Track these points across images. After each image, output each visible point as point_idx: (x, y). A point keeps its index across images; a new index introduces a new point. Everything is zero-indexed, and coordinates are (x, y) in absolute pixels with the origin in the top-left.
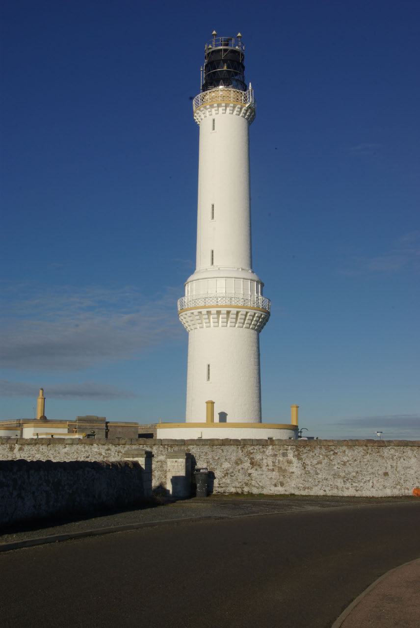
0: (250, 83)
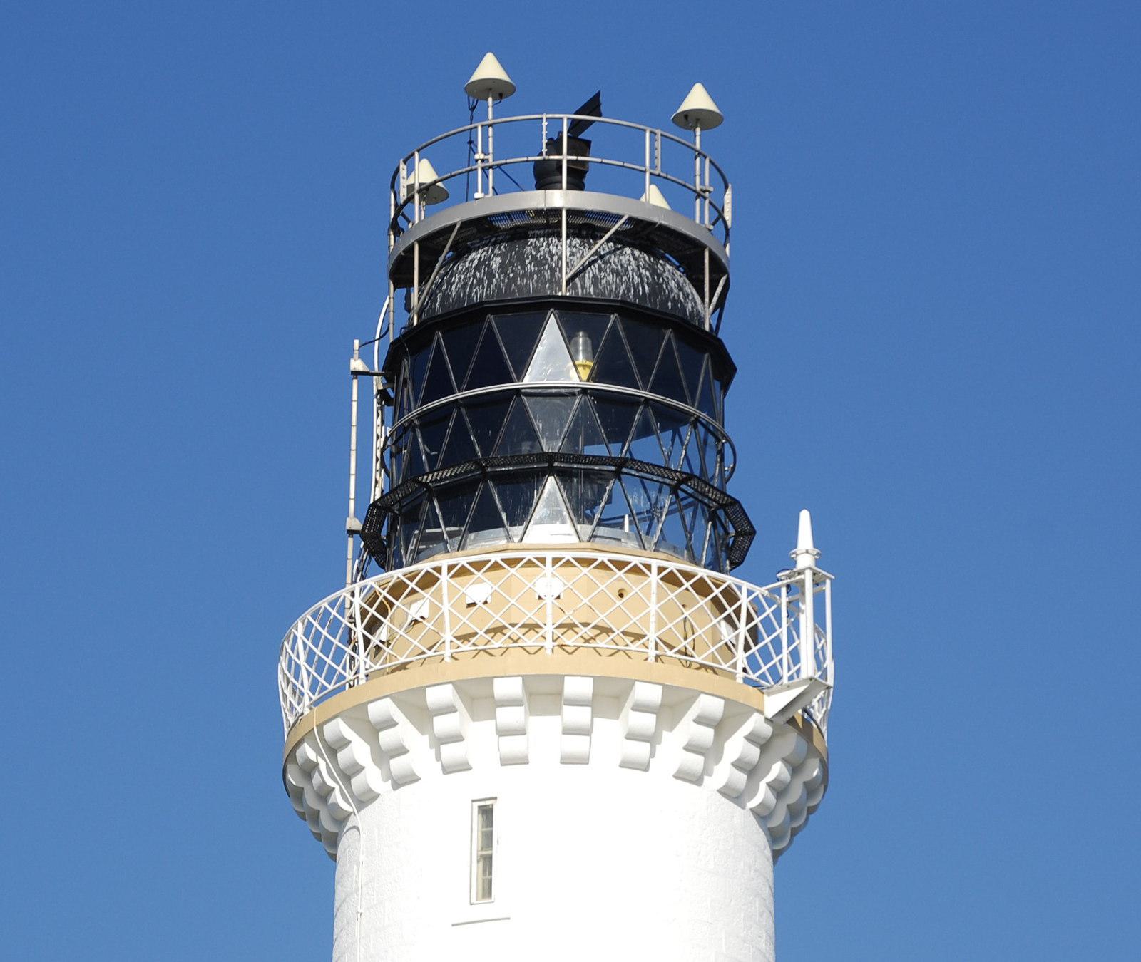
0: (805, 517)
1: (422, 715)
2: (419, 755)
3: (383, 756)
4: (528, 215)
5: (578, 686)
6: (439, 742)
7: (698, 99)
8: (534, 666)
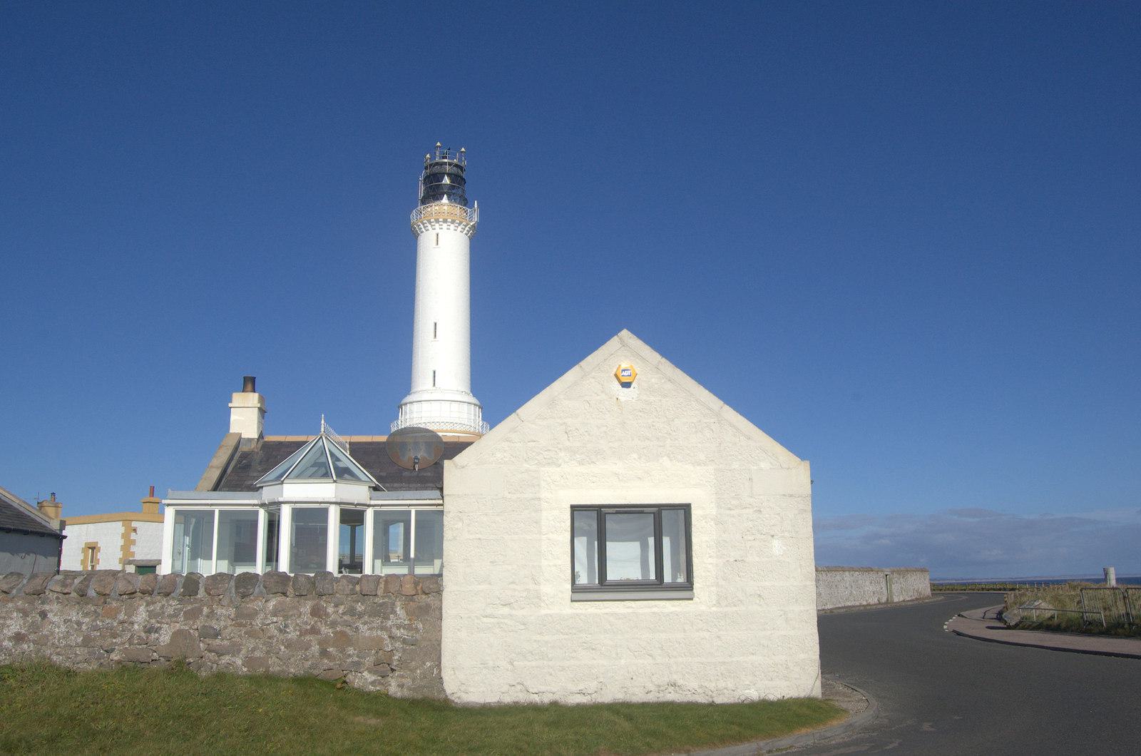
1: (430, 223)
2: (429, 227)
3: (425, 227)
4: (334, 686)
5: (450, 220)
6: (432, 226)
7: (463, 149)
8: (445, 217)
